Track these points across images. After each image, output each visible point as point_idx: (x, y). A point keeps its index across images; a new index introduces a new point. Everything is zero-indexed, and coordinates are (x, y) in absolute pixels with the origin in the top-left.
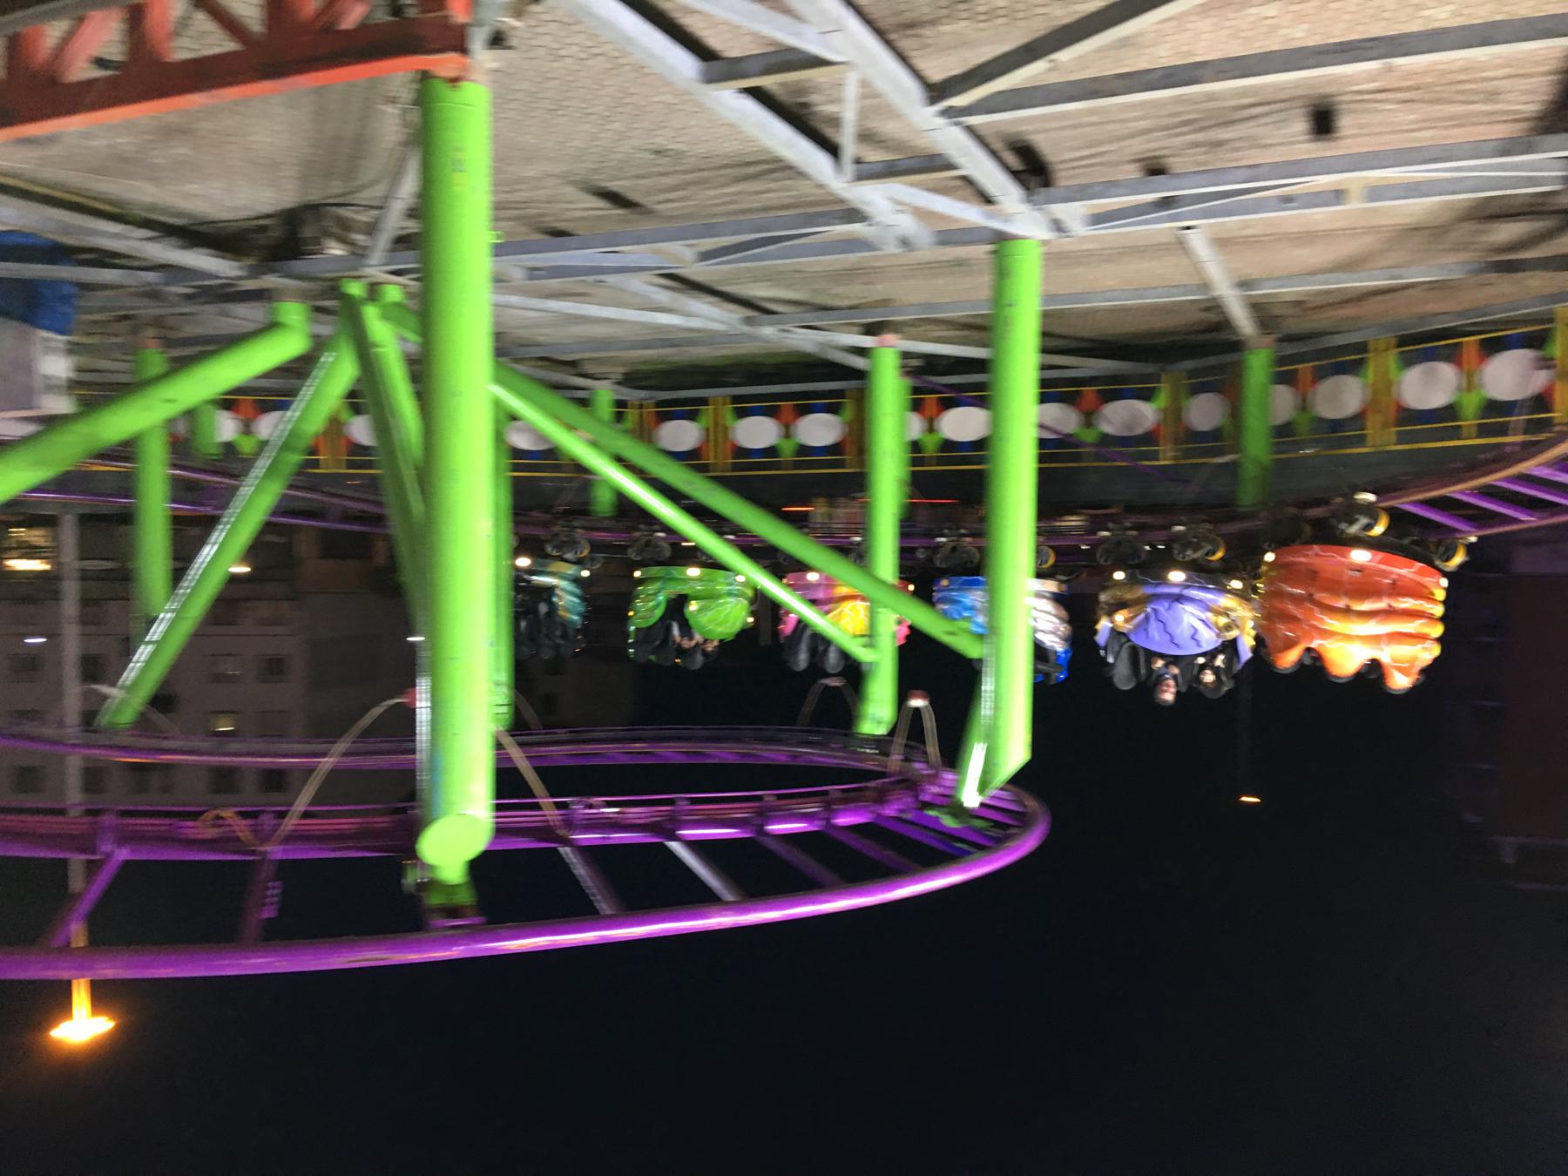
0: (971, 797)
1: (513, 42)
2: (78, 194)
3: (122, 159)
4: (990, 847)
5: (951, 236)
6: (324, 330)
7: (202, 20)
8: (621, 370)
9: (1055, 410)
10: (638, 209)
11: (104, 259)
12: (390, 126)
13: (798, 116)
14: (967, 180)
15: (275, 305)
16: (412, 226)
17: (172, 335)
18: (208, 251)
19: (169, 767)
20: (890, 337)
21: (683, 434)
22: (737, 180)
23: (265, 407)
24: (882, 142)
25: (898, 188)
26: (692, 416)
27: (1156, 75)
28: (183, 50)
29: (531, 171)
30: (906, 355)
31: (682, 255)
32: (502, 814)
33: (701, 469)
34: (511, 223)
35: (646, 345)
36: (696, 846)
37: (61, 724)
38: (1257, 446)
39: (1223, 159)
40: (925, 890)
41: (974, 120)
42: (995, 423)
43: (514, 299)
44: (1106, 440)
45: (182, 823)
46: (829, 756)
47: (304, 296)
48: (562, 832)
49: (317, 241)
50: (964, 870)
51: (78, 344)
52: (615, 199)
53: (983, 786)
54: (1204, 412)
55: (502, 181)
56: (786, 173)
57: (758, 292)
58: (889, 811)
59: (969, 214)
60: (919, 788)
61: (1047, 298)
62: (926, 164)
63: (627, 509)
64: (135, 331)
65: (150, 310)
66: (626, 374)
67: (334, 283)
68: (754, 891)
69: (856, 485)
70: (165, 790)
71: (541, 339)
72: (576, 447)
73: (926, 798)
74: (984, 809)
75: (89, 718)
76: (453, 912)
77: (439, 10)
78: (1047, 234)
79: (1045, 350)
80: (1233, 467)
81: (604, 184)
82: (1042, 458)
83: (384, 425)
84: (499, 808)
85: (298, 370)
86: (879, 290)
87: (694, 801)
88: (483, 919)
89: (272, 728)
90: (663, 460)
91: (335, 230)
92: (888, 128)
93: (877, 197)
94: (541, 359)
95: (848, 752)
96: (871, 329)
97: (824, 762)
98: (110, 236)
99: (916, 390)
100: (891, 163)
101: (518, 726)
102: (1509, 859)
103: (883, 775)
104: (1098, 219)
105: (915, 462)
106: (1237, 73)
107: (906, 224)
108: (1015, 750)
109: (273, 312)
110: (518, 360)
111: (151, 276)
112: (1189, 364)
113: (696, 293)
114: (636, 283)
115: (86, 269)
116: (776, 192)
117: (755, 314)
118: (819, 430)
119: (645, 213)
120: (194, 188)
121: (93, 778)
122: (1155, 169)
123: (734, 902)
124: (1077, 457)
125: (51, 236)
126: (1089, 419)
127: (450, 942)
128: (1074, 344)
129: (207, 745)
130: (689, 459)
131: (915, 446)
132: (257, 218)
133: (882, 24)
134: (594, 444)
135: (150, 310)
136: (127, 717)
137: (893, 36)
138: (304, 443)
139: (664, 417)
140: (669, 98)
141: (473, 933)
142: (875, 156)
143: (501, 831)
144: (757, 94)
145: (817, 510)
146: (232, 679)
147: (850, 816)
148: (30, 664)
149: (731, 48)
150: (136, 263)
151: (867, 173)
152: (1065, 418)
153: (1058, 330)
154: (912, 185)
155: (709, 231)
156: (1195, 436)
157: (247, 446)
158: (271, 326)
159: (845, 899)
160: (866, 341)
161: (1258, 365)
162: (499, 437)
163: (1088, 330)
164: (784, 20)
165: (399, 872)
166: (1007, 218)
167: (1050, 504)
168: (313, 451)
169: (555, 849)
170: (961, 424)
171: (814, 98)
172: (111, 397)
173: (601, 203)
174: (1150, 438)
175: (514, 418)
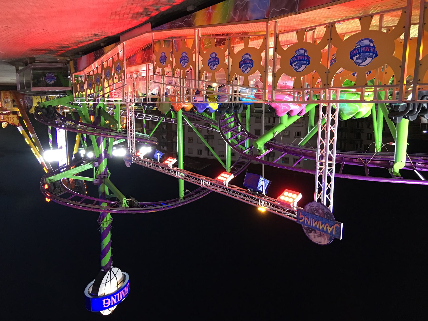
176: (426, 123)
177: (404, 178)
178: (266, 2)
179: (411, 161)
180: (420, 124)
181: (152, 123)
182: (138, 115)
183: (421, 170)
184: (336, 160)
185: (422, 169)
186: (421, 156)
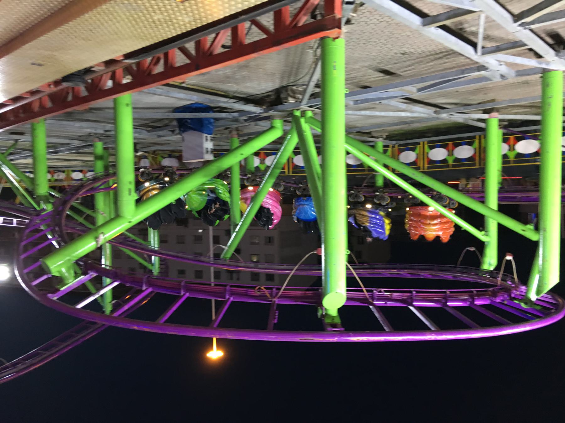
0: (533, 296)
1: (353, 21)
2: (222, 91)
3: (228, 77)
4: (542, 317)
6: (288, 128)
7: (254, 28)
8: (387, 134)
10: (394, 75)
11: (222, 110)
12: (310, 56)
14: (531, 50)
15: (272, 121)
16: (318, 90)
17: (241, 133)
18: (253, 105)
19: (239, 272)
20: (495, 114)
21: (410, 156)
22: (432, 61)
23: (268, 155)
24: (493, 39)
25: (500, 56)
26: (413, 150)
28: (248, 40)
29: (357, 66)
30: (501, 121)
31: (412, 91)
33: (418, 169)
34: (349, 85)
36: (419, 308)
37: (209, 257)
40: (513, 332)
41: (533, 27)
42: (542, 145)
45: (249, 290)
46: (469, 278)
47: (281, 117)
48: (371, 300)
49: (286, 98)
50: (532, 325)
51: (214, 138)
52: (387, 72)
53: (538, 292)
55: (348, 72)
56: (453, 55)
57: (440, 101)
58: (498, 300)
59: (532, 63)
60: (511, 292)
63: (388, 184)
64: (230, 132)
65: (235, 125)
66: (387, 136)
67: (291, 112)
68: (443, 327)
70: (238, 279)
72: (370, 162)
73: (513, 295)
74: (538, 301)
75: (217, 256)
76: (334, 325)
77: (333, 14)
81: (383, 68)
83: (307, 159)
84: (348, 290)
85: (280, 141)
87: (417, 292)
88: (343, 329)
89: (269, 260)
90: (404, 166)
91: (291, 94)
92: (495, 33)
93: (491, 61)
94: (357, 132)
95: (478, 276)
96: (486, 112)
97: (467, 280)
98: (223, 102)
99: (504, 134)
101: (350, 260)
103: (496, 286)
105: (504, 163)
107: (504, 69)
109: (272, 123)
111: (236, 115)
113: (417, 104)
114: (393, 102)
115: (97, 120)
117: (438, 109)
119: (398, 76)
120: (248, 84)
121: (217, 275)
123: (434, 331)
125: (206, 104)
127: (334, 336)
129: (252, 265)
130: (413, 165)
131: (505, 156)
132: (267, 92)
134: (376, 161)
135: (235, 125)
136: (229, 256)
138: (282, 166)
139: (400, 151)
140: (408, 33)
141: (341, 334)
142: (489, 45)
143: (348, 299)
144: (444, 28)
145: (462, 183)
146: (258, 244)
147: (481, 301)
148: (199, 238)
149: (431, 11)
151: (486, 51)
154: (507, 54)
155: (423, 80)
157: (262, 167)
158: (272, 128)
160: (485, 116)
165: (316, 311)
166: (548, 63)
168: (283, 168)
169: (368, 306)
172: (257, 151)
173: (382, 75)
175: (348, 153)
177: (345, 330)
178: (203, 212)
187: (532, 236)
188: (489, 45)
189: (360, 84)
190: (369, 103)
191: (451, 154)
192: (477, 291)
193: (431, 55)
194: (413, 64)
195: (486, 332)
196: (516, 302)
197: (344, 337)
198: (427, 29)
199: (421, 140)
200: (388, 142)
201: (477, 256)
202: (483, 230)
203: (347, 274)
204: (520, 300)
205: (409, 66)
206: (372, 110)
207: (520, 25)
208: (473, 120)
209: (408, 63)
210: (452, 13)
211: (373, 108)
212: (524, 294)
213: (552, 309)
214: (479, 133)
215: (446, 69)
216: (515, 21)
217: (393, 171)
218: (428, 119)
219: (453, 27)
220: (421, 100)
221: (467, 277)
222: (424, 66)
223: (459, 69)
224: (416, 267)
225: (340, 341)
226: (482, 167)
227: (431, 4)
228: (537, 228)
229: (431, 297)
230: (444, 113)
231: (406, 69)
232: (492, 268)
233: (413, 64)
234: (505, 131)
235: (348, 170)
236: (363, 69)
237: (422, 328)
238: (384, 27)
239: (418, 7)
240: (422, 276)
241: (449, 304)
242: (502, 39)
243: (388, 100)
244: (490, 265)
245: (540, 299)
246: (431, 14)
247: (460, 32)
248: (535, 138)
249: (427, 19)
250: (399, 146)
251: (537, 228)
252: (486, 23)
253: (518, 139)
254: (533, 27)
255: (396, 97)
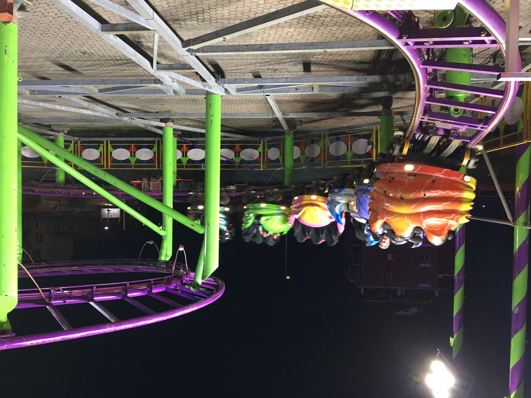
1: (28, 9)
5: (191, 91)
9: (225, 151)
10: (76, 72)
13: (137, 46)
14: (197, 73)
20: (170, 124)
21: (93, 154)
26: (97, 148)
27: (258, 46)
29: (33, 55)
31: (93, 90)
32: (20, 295)
33: (101, 167)
34: (24, 73)
35: (78, 121)
36: (99, 303)
38: (289, 163)
39: (277, 75)
41: (198, 54)
43: (26, 101)
44: (242, 161)
48: (47, 301)
50: (197, 306)
52: (67, 68)
54: (273, 154)
56: (132, 64)
59: (198, 85)
61: (223, 114)
62: (184, 67)
63: (69, 179)
68: (122, 318)
69: (159, 174)
71: (35, 116)
78: (224, 94)
79: (222, 131)
80: (283, 171)
82: (221, 167)
86: (167, 107)
87: (97, 287)
88: (14, 334)
92: (169, 53)
93: (165, 76)
96: (162, 121)
100: (170, 65)
101: (25, 260)
102: (362, 292)
103: (171, 274)
104: (239, 90)
105: (178, 167)
106: (282, 49)
107: (176, 86)
108: (214, 264)
110: (25, 124)
112: (269, 138)
114: (74, 98)
116: (129, 71)
117: (120, 112)
118: (145, 154)
122: (257, 76)
124: (131, 166)
126: (237, 154)
128: (231, 129)
130: (96, 163)
131: (179, 161)
133: (167, 18)
134: (57, 156)
137: (170, 23)
139: (84, 148)
140: (89, 35)
141: (12, 340)
143: (20, 301)
144: (122, 37)
149: (113, 21)
150: (73, 104)
151: (160, 67)
152: (230, 154)
153: (226, 124)
154: (179, 73)
155: (103, 82)
156: (269, 161)
159: (157, 318)
160: (163, 125)
161: (289, 140)
162: (19, 152)
163: (237, 125)
164: (132, 13)
166: (210, 87)
167: (224, 183)
170: (195, 154)
171: (143, 40)
174: (257, 161)
175: (23, 145)
176: (107, 217)
177: (16, 336)
179: (38, 286)
180: (100, 219)
181: (390, 19)
182: (439, 193)
183: (64, 303)
184: (494, 184)
185: (64, 302)
186: (86, 265)
187: (200, 230)
188: (163, 62)
189: (36, 74)
190: (48, 95)
191: (133, 154)
192: (154, 281)
193: (112, 60)
194: (94, 65)
195: (160, 317)
196: (186, 286)
197: (17, 343)
198: (107, 36)
199: (104, 139)
200: (70, 138)
201: (287, 235)
202: (161, 225)
203: (19, 274)
204: (190, 285)
205: (90, 66)
206: (52, 102)
207: (187, 51)
208: (152, 126)
209: (89, 63)
210: (129, 26)
211: (53, 101)
212: (193, 279)
213: (214, 290)
214: (158, 139)
215: (125, 76)
216: (184, 47)
217: (76, 167)
218: (110, 120)
219: (131, 38)
220: (104, 101)
221: (146, 269)
222: (104, 69)
223: (138, 78)
224: (99, 262)
225: (11, 348)
226: (161, 169)
227: (110, 12)
228: (203, 224)
229: (111, 290)
230: (125, 116)
231: (87, 68)
232: (168, 259)
233: (94, 65)
234: (179, 140)
235: (22, 163)
236: (40, 60)
237: (103, 322)
238: (50, 22)
239: (98, 12)
240: (104, 270)
241: (128, 295)
242: (174, 59)
243: (69, 95)
244: (166, 256)
245: (205, 282)
246: (110, 22)
247: (138, 44)
248: (203, 148)
249: (106, 25)
250: (80, 143)
251: (203, 224)
252: (159, 42)
253: (190, 148)
254: (198, 54)
255: (78, 94)
